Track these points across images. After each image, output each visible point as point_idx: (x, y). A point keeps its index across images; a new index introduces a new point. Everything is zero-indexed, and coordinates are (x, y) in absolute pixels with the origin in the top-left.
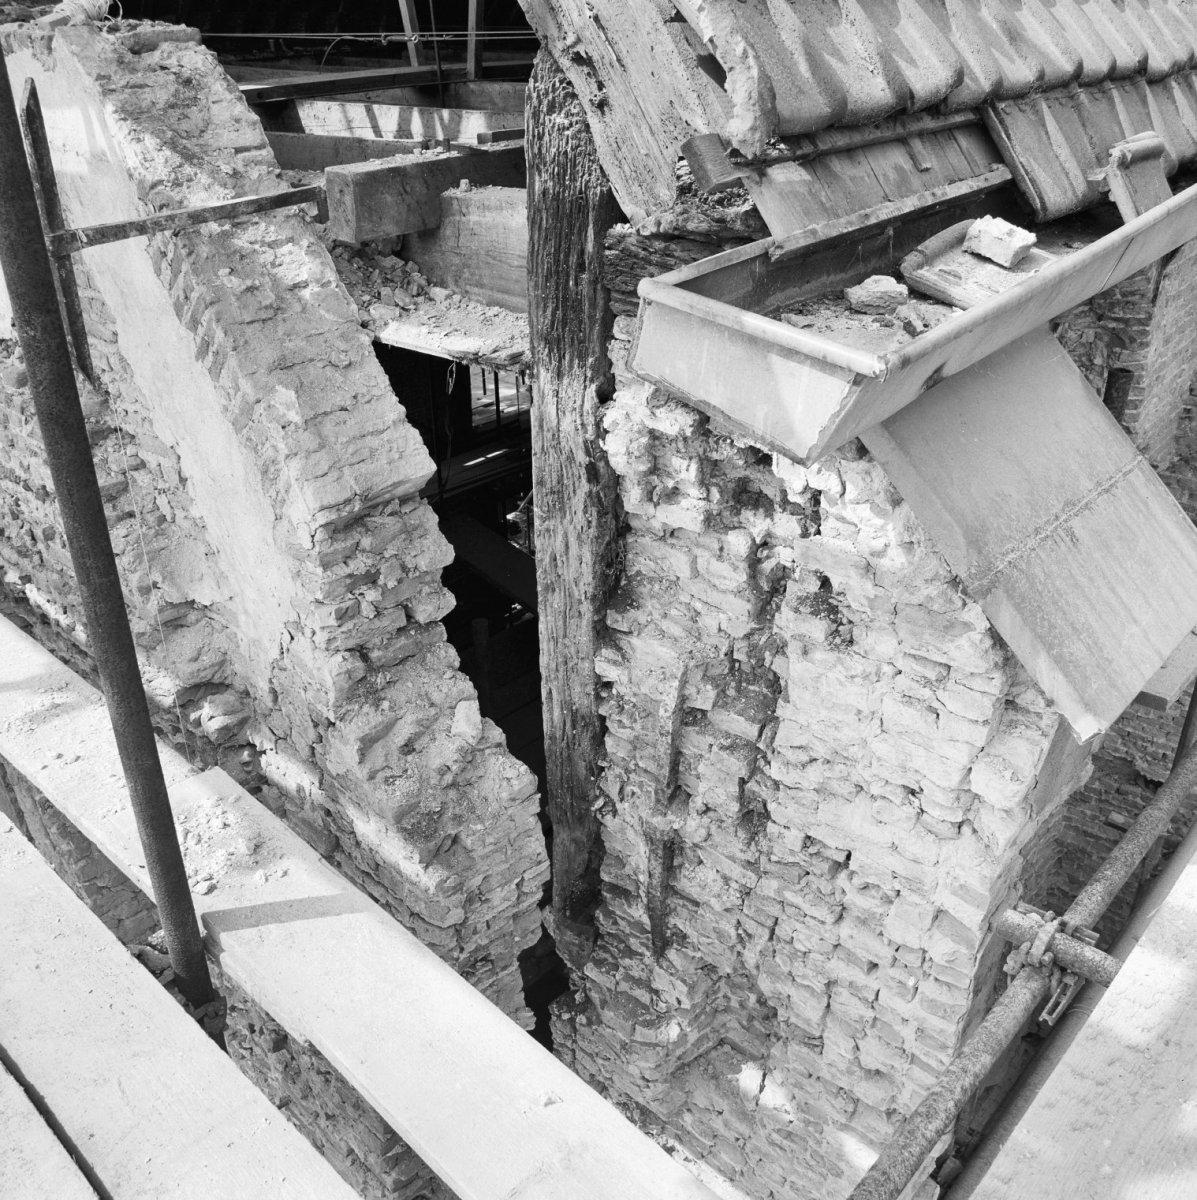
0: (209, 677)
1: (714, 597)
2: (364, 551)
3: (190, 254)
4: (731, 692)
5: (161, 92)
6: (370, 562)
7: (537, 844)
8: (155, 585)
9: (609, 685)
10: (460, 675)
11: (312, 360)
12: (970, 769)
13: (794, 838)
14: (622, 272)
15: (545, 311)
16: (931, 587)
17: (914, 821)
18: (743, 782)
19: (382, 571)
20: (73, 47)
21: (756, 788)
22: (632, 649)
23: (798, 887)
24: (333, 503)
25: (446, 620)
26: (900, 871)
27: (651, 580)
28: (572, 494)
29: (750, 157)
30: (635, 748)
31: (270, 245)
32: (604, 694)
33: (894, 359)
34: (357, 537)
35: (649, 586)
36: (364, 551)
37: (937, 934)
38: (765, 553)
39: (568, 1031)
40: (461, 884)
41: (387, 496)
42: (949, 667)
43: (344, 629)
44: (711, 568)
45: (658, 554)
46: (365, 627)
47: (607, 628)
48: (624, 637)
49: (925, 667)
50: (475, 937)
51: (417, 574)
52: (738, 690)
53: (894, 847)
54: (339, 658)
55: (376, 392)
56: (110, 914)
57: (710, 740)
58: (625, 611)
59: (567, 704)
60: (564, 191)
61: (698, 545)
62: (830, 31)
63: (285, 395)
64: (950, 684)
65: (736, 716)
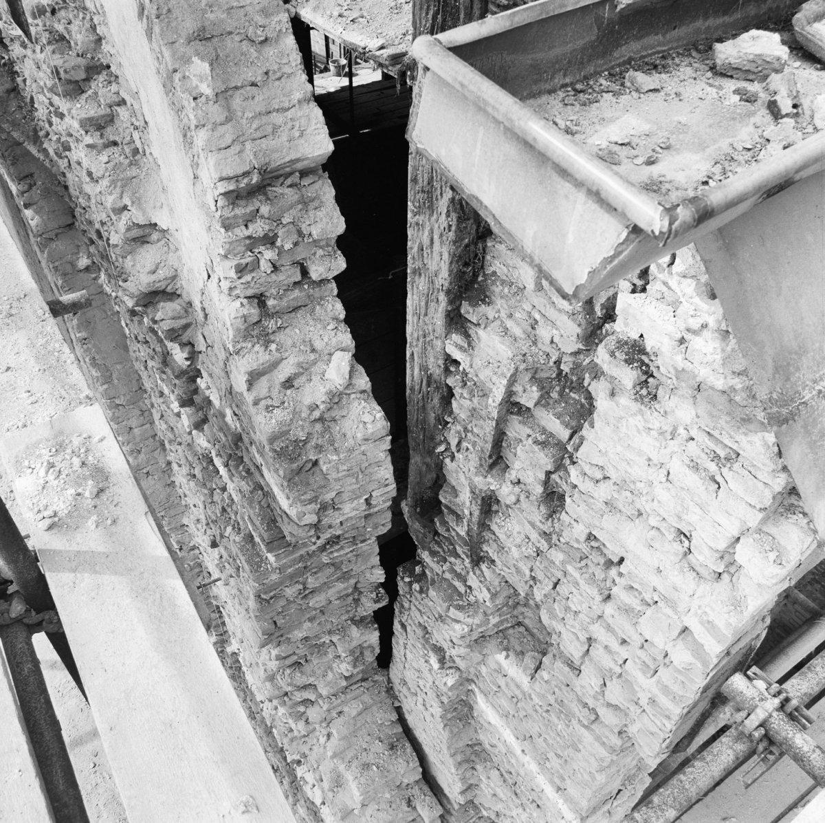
0: (163, 287)
2: (262, 217)
4: (555, 395)
6: (267, 228)
7: (386, 472)
8: (125, 208)
9: (456, 363)
10: (343, 327)
11: (230, 33)
12: (739, 538)
13: (580, 531)
15: (427, 14)
16: (737, 380)
17: (680, 557)
18: (548, 473)
19: (280, 234)
21: (558, 480)
22: (478, 338)
23: (579, 565)
26: (660, 588)
27: (503, 282)
28: (439, 197)
30: (472, 415)
32: (452, 369)
34: (257, 204)
36: (262, 217)
37: (680, 643)
39: (407, 589)
40: (316, 497)
41: (288, 169)
42: (739, 455)
43: (243, 280)
45: (510, 263)
46: (262, 280)
47: (460, 316)
49: (717, 445)
52: (561, 394)
53: (659, 571)
54: (237, 304)
55: (287, 69)
57: (529, 431)
59: (424, 368)
63: (200, 67)
64: (736, 466)
65: (553, 418)
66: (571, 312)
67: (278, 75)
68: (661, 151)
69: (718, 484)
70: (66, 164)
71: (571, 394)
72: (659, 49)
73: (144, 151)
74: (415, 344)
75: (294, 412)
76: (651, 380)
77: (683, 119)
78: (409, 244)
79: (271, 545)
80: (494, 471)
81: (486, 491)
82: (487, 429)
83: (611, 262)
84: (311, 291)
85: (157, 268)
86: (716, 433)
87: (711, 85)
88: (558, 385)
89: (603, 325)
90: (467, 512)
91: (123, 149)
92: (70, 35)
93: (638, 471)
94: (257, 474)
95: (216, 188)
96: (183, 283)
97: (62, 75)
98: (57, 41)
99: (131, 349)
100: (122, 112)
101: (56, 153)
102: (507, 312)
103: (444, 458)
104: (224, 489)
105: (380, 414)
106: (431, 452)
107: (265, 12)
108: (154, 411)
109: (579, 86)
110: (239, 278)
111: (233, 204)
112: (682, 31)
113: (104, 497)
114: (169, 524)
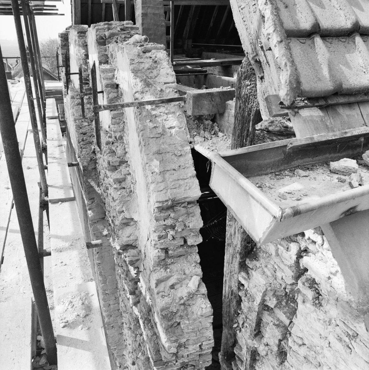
0: (131, 243)
1: (282, 266)
2: (171, 218)
3: (140, 114)
4: (284, 303)
5: (147, 63)
6: (172, 222)
7: (210, 333)
8: (123, 211)
9: (243, 285)
10: (199, 266)
11: (169, 152)
14: (260, 140)
18: (280, 341)
20: (127, 51)
22: (252, 275)
24: (161, 201)
25: (198, 246)
27: (263, 252)
29: (287, 106)
31: (166, 114)
32: (241, 288)
33: (288, 211)
35: (262, 254)
36: (171, 218)
38: (305, 254)
41: (183, 201)
43: (160, 242)
44: (283, 255)
46: (168, 242)
47: (246, 265)
48: (250, 270)
49: (348, 329)
50: (182, 359)
51: (189, 229)
52: (287, 303)
54: (157, 251)
55: (187, 165)
56: (107, 302)
57: (272, 319)
58: (252, 260)
59: (230, 287)
60: (246, 108)
61: (280, 244)
62: (347, 56)
63: (156, 163)
66: (290, 266)
67: (184, 167)
68: (303, 196)
69: (351, 349)
70: (106, 195)
71: (291, 304)
72: (311, 163)
73: (134, 192)
74: (227, 276)
75: (173, 299)
76: (320, 297)
77: (314, 186)
78: (227, 233)
79: (156, 363)
80: (257, 338)
81: (252, 348)
82: (253, 316)
83: (269, 229)
84: (187, 249)
85: (130, 235)
86: (346, 322)
87: (328, 176)
88: (285, 299)
89: (304, 273)
90: (245, 359)
91: (126, 190)
92: (117, 151)
93: (316, 341)
94: (155, 328)
95: (155, 205)
96: (139, 242)
97: (111, 164)
98: (112, 153)
99: (116, 270)
100: (129, 177)
101: (104, 191)
102: (265, 265)
103: (236, 331)
104: (141, 335)
105: (209, 305)
106: (231, 328)
107: (182, 146)
108: (120, 298)
109: (277, 173)
110: (159, 240)
111: (160, 211)
112: (320, 157)
113: (87, 318)
114: (117, 353)
